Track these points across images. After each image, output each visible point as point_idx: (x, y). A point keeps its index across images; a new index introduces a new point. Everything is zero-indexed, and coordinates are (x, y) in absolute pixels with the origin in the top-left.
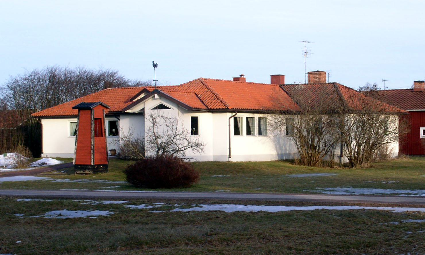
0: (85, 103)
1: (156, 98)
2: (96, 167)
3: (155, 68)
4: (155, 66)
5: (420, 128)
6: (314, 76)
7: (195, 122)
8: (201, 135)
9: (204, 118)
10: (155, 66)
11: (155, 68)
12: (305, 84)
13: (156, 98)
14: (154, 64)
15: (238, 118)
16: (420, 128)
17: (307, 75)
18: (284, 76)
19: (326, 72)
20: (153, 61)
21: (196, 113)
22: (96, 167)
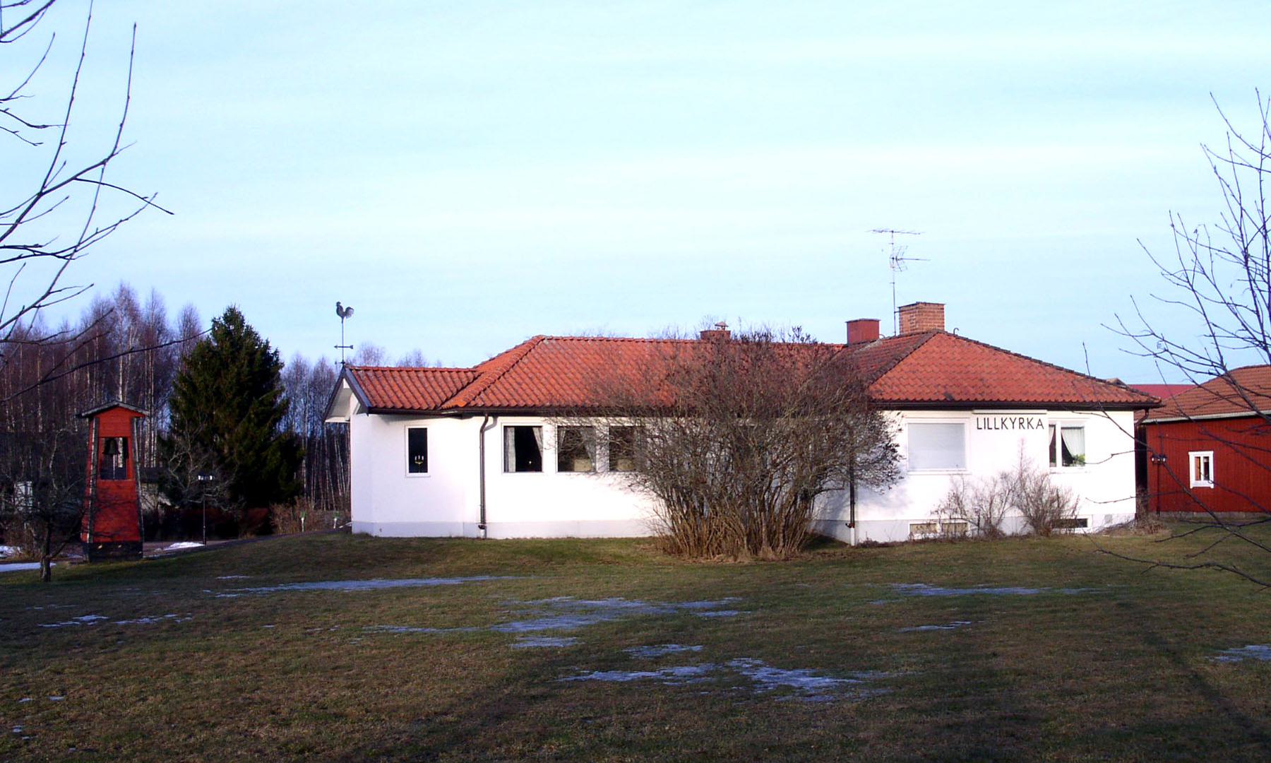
0: (624, 427)
1: (1127, 419)
2: (100, 547)
3: (343, 318)
4: (343, 312)
5: (1190, 453)
6: (909, 316)
7: (418, 444)
8: (934, 510)
9: (439, 431)
10: (343, 312)
11: (343, 318)
12: (895, 337)
13: (1127, 419)
14: (339, 309)
15: (534, 429)
16: (1190, 453)
17: (897, 314)
18: (878, 321)
19: (943, 305)
20: (338, 304)
21: (416, 419)
22: (100, 547)
